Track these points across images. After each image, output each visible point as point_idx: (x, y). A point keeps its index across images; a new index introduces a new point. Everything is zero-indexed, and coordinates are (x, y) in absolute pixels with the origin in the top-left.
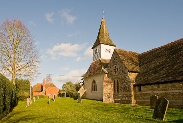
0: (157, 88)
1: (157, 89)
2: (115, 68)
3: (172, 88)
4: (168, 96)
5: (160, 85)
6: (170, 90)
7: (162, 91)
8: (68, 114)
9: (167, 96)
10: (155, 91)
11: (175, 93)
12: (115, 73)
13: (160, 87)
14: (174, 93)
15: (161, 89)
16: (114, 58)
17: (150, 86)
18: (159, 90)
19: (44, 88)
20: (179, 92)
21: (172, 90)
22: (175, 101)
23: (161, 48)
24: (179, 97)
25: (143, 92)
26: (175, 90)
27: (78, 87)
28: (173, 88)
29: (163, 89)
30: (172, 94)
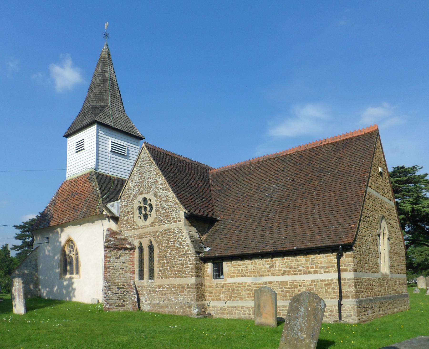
0: (268, 266)
1: (269, 271)
2: (142, 205)
3: (308, 268)
5: (277, 260)
6: (305, 273)
10: (262, 276)
11: (318, 282)
12: (142, 218)
14: (313, 281)
15: (280, 271)
16: (140, 174)
17: (248, 262)
18: (273, 275)
20: (328, 280)
21: (310, 273)
24: (326, 291)
25: (230, 280)
26: (316, 272)
28: (312, 268)
29: (285, 271)
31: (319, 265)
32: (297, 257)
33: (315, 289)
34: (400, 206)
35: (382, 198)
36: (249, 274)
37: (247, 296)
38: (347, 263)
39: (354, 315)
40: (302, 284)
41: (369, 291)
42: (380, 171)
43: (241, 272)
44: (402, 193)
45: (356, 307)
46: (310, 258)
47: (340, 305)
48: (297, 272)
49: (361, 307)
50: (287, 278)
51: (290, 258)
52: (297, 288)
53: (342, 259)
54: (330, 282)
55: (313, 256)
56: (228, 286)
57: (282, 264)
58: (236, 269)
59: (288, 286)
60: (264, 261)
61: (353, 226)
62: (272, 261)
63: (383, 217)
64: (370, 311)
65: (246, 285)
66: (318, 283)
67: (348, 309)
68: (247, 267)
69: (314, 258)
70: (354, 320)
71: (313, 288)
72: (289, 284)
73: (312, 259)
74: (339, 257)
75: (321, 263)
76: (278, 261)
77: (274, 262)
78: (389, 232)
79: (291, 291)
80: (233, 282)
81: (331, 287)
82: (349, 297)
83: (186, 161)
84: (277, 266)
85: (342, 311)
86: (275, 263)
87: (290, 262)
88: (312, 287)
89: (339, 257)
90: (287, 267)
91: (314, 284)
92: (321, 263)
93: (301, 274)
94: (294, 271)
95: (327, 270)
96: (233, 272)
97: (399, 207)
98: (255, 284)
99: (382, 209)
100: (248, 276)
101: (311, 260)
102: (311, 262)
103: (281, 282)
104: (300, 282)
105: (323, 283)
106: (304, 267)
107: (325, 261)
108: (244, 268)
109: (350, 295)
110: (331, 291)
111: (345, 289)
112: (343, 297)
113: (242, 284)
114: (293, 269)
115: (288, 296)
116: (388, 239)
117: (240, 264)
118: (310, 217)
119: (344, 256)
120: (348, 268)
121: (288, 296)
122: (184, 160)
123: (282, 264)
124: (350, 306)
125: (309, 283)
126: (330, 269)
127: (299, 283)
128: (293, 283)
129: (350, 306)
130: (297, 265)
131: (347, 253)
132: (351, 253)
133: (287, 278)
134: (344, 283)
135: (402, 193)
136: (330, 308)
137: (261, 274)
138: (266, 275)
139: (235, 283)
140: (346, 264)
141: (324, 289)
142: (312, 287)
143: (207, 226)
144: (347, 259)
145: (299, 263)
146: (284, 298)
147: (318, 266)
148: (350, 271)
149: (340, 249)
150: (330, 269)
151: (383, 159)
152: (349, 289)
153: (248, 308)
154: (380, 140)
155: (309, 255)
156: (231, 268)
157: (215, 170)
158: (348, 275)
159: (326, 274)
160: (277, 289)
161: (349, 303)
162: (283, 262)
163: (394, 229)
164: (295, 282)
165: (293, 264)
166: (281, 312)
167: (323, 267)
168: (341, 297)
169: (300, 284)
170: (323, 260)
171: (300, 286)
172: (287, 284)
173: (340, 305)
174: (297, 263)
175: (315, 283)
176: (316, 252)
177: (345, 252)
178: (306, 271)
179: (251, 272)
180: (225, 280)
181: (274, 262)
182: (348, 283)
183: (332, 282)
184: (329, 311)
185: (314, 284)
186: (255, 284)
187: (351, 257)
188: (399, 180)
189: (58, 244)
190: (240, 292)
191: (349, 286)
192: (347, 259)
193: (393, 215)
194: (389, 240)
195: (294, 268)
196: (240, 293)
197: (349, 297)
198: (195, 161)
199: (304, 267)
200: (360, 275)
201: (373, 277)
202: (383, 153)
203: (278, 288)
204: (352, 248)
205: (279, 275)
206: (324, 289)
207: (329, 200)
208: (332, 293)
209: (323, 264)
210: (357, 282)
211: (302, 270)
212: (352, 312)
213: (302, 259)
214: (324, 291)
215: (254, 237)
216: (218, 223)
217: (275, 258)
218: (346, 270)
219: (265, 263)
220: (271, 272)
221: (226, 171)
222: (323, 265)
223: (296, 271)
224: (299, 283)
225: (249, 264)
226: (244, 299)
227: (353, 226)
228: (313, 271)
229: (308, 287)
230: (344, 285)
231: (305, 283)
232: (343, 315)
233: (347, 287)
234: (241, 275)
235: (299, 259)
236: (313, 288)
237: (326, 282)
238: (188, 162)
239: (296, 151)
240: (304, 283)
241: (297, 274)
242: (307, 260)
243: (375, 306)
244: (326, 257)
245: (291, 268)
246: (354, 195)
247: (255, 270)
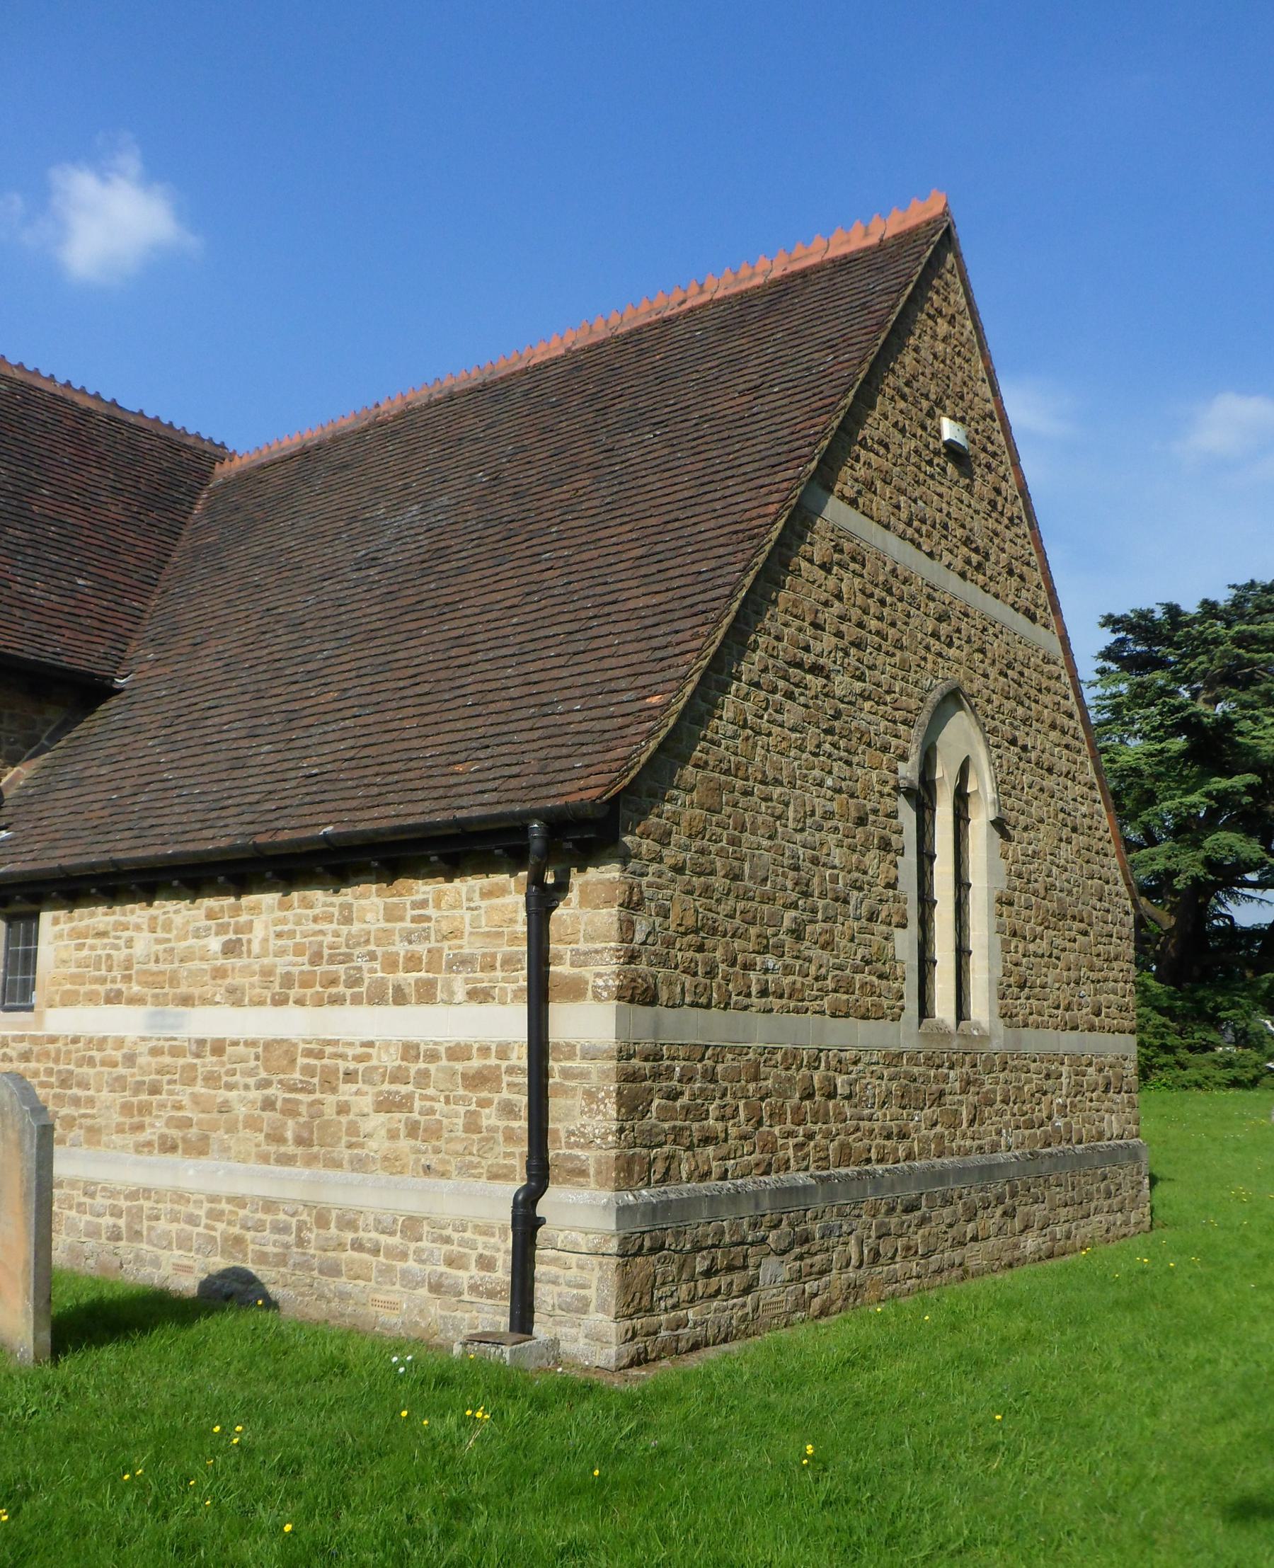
1: (219, 973)
4: (343, 1109)
5: (254, 909)
6: (377, 997)
7: (269, 1011)
8: (1214, 779)
9: (330, 1099)
10: (186, 1001)
11: (433, 1056)
13: (258, 932)
14: (410, 1051)
17: (136, 913)
18: (235, 997)
19: (225, 1115)
20: (484, 1051)
21: (400, 998)
22: (410, 1204)
23: (284, 460)
24: (472, 1125)
25: (58, 1020)
26: (427, 993)
27: (1231, 1521)
28: (413, 962)
29: (288, 981)
30: (394, 1079)
31: (447, 949)
32: (349, 895)
33: (417, 1104)
34: (1241, 733)
35: (969, 593)
36: (136, 988)
37: (117, 1118)
38: (590, 938)
39: (602, 1308)
40: (361, 1067)
41: (789, 1134)
42: (946, 436)
43: (103, 972)
44: (1262, 688)
45: (613, 1246)
46: (408, 900)
47: (526, 1224)
48: (341, 989)
49: (645, 1247)
50: (296, 1023)
51: (318, 896)
52: (334, 1090)
53: (561, 913)
54: (493, 1061)
55: (423, 889)
56: (47, 1055)
57: (279, 935)
58: (85, 952)
59: (297, 1075)
60: (202, 912)
61: (655, 700)
62: (236, 911)
63: (954, 698)
64: (773, 1270)
65: (118, 1055)
66: (432, 1067)
67: (573, 1258)
68: (129, 943)
69: (423, 904)
70: (595, 1337)
71: (410, 1097)
72: (301, 1061)
73: (416, 905)
74: (542, 903)
75: (454, 934)
76: (264, 913)
77: (244, 918)
78: (1004, 788)
79: (303, 1109)
80: (71, 1033)
81: (496, 1098)
82: (583, 1173)
83: (74, 404)
84: (256, 947)
85: (540, 1270)
86: (249, 927)
87: (315, 919)
88: (404, 1089)
89: (542, 903)
90: (299, 950)
91: (414, 1068)
92: (454, 934)
93: (357, 1000)
94: (328, 981)
95: (484, 979)
96: (74, 970)
97: (1239, 739)
98: (155, 1052)
99: (953, 652)
100: (133, 1001)
101: (410, 913)
102: (408, 924)
103: (268, 1045)
104: (350, 1052)
105: (459, 1066)
106: (372, 956)
107: (475, 923)
108: (117, 948)
109: (588, 1156)
110: (493, 1121)
111: (568, 1115)
112: (553, 1172)
113: (102, 1043)
114: (325, 967)
115: (289, 1135)
116: (999, 825)
117: (101, 927)
118: (480, 656)
119: (573, 895)
120: (587, 973)
121: (289, 1135)
122: (62, 399)
123: (279, 935)
124: (580, 1238)
125: (389, 1060)
126: (499, 974)
127: (342, 1056)
128: (320, 1055)
129: (580, 1238)
130: (342, 940)
131: (592, 873)
132: (610, 872)
133: (296, 1023)
134: (566, 1074)
135: (1262, 688)
136: (481, 1239)
137: (183, 989)
138: (206, 1001)
139: (75, 1040)
140: (582, 946)
141: (462, 1110)
142: (404, 1089)
143: (54, 714)
144: (590, 911)
145: (356, 927)
146: (272, 1148)
147: (440, 950)
148: (597, 997)
149: (546, 844)
150: (499, 974)
151: (986, 390)
152: (586, 1118)
153: (113, 1194)
154: (965, 282)
155: (401, 883)
156: (67, 947)
157: (237, 462)
158: (588, 1026)
159: (475, 1008)
160: (247, 1087)
161: (581, 1215)
162: (284, 921)
163: (1050, 782)
164: (329, 1050)
165: (331, 934)
166: (249, 1235)
167: (464, 962)
168: (539, 1172)
169: (352, 1065)
170: (468, 916)
171: (350, 1076)
172: (293, 1061)
173: (526, 1224)
174: (344, 929)
175: (422, 1065)
176: (426, 860)
177: (582, 869)
178: (382, 983)
179: (153, 980)
180: (40, 1023)
181: (244, 918)
182: (583, 1075)
183: (504, 1064)
184: (474, 1255)
185: (414, 1068)
186: (155, 1052)
187: (608, 903)
188: (1253, 636)
189: (175, 883)
190: (91, 1093)
191: (590, 1095)
192: (587, 914)
193: (1045, 698)
194: (1006, 836)
195: (331, 961)
196: (91, 1102)
197: (583, 1173)
198: (141, 414)
199: (372, 956)
200: (687, 1026)
201: (832, 1042)
202: (986, 357)
203: (251, 1081)
204: (614, 840)
205: (261, 1003)
206: (462, 1110)
207: (601, 562)
208: (500, 1137)
209: (464, 942)
210: (640, 1078)
211: (366, 975)
212: (593, 1277)
213: (367, 902)
214: (460, 1122)
215: (206, 769)
216: (114, 701)
217: (251, 893)
218: (576, 990)
219: (204, 923)
220: (228, 981)
221: (262, 467)
222: (466, 951)
223: (334, 982)
224: (342, 1056)
225: (138, 928)
226: (104, 1138)
227: (655, 700)
228: (417, 981)
229: (386, 1087)
230: (566, 1092)
231: (374, 1062)
232: (544, 1294)
233: (579, 1102)
234: (101, 989)
235: (356, 903)
236: (410, 1097)
237: (476, 1063)
238: (88, 412)
239: (568, 350)
240: (368, 1057)
241: (337, 1000)
242: (392, 915)
243: (827, 1233)
244: (485, 894)
245: (316, 958)
246: (726, 530)
247: (162, 967)
